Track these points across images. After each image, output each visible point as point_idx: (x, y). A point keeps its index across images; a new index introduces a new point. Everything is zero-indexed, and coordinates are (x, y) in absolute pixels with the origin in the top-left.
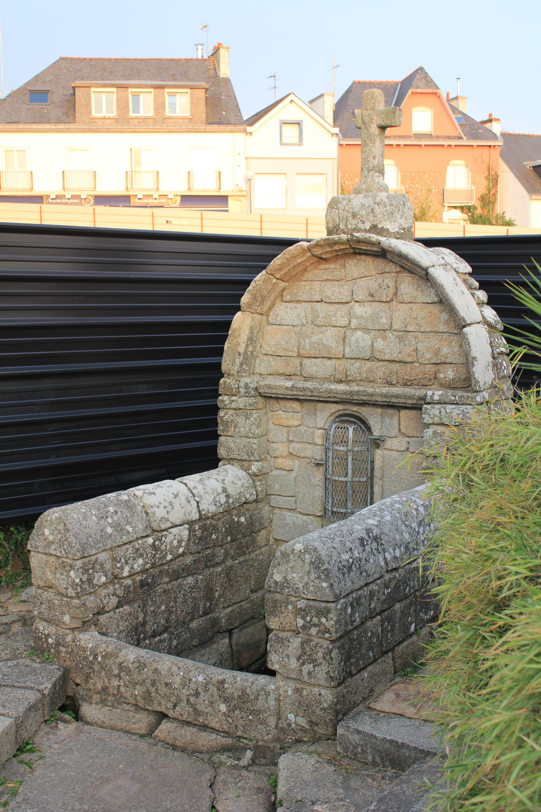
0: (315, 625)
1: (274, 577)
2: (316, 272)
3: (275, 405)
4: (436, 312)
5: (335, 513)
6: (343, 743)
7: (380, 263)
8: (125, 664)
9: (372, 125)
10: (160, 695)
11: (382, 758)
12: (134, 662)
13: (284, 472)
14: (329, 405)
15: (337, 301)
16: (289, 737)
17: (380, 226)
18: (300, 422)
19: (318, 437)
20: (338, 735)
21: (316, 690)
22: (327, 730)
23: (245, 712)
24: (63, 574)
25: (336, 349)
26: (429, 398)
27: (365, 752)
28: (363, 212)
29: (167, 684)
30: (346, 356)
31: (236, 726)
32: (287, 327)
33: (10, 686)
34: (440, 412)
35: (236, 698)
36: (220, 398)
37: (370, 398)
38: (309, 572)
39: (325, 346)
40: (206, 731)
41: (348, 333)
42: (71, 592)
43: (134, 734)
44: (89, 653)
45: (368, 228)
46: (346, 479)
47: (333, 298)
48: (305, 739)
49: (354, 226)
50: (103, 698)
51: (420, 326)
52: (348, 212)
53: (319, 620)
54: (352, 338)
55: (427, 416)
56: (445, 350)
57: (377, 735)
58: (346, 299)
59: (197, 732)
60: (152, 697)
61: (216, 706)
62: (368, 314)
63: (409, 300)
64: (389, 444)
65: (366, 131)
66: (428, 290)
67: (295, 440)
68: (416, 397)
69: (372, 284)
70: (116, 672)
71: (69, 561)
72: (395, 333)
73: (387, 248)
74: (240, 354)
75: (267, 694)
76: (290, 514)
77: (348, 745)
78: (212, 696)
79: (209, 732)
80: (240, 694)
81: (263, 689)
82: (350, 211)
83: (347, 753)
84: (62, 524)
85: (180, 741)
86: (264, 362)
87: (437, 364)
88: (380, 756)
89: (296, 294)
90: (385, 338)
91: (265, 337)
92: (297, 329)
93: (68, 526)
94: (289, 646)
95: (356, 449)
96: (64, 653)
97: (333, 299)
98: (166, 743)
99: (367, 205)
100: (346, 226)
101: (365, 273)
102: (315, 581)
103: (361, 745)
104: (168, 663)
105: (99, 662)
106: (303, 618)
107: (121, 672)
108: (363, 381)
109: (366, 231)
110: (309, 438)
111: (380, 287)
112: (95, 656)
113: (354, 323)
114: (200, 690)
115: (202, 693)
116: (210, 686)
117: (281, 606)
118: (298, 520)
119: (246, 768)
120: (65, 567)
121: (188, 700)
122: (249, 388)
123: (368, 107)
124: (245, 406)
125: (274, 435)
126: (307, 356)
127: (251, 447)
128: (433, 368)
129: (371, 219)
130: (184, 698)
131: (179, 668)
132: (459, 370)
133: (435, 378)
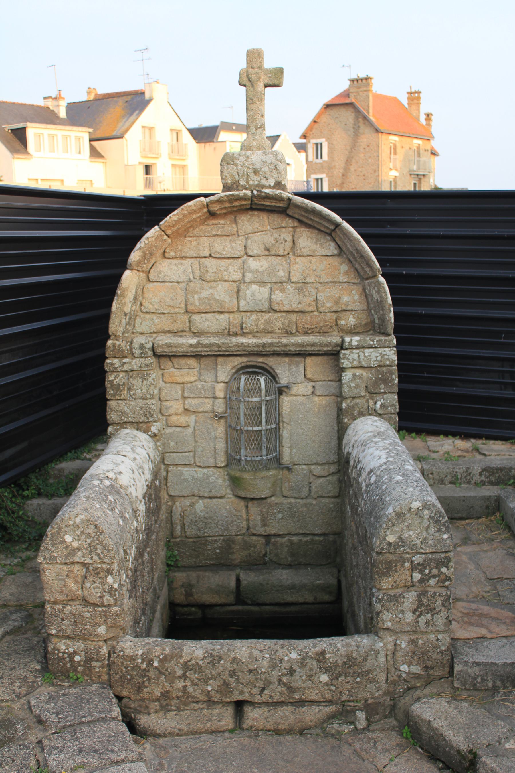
0: (434, 576)
1: (387, 538)
2: (202, 227)
3: (166, 363)
4: (336, 263)
5: (249, 461)
6: (461, 679)
7: (277, 219)
8: (193, 662)
9: (259, 83)
10: (242, 684)
11: (502, 681)
12: (205, 657)
13: (179, 429)
14: (231, 358)
15: (229, 256)
16: (399, 687)
17: (283, 183)
18: (196, 378)
19: (220, 390)
20: (455, 672)
21: (432, 637)
22: (443, 670)
23: (352, 676)
24: (95, 582)
25: (230, 303)
26: (347, 344)
27: (485, 680)
28: (266, 169)
29: (250, 671)
30: (241, 310)
31: (341, 692)
32: (171, 284)
33: (77, 724)
34: (359, 356)
35: (340, 665)
36: (108, 361)
37: (283, 349)
38: (428, 527)
39: (217, 301)
40: (305, 706)
41: (243, 287)
42: (107, 599)
43: (223, 732)
44: (140, 661)
45: (272, 184)
46: (259, 428)
47: (224, 253)
48: (418, 685)
49: (257, 183)
50: (164, 703)
51: (320, 277)
52: (249, 168)
53: (439, 570)
54: (248, 292)
55: (346, 361)
56: (345, 299)
57: (498, 662)
58: (239, 254)
59: (295, 709)
60: (231, 688)
61: (316, 679)
62: (264, 268)
63: (308, 253)
64: (295, 390)
65: (252, 89)
66: (328, 244)
67: (191, 396)
68: (332, 344)
69: (269, 239)
70: (180, 672)
71: (104, 566)
72: (293, 285)
73: (300, 204)
74: (126, 315)
75: (377, 653)
76: (187, 469)
77: (467, 678)
78: (311, 670)
79: (308, 705)
80: (345, 660)
81: (371, 650)
82: (251, 167)
83: (465, 686)
84: (92, 527)
85: (284, 724)
86: (145, 320)
87: (336, 312)
88: (501, 680)
89: (181, 250)
90: (283, 291)
91: (146, 295)
92: (183, 285)
93: (101, 527)
94: (403, 602)
95: (268, 398)
96: (99, 668)
97: (224, 254)
98: (266, 730)
99: (269, 162)
100: (248, 182)
101: (259, 228)
102: (435, 534)
103: (481, 675)
104: (244, 649)
105: (156, 668)
106: (421, 572)
107: (186, 672)
108: (260, 332)
109: (270, 187)
110: (207, 393)
111: (277, 242)
112: (150, 663)
113: (249, 277)
114: (294, 667)
115: (298, 670)
116: (308, 660)
117: (395, 566)
118: (197, 473)
119: (367, 729)
120: (99, 573)
121: (280, 681)
122: (146, 348)
123: (255, 66)
124: (141, 367)
125: (166, 393)
126: (196, 311)
127: (150, 408)
128: (334, 316)
129: (276, 176)
130: (275, 680)
131: (261, 651)
132: (360, 316)
133: (337, 325)
